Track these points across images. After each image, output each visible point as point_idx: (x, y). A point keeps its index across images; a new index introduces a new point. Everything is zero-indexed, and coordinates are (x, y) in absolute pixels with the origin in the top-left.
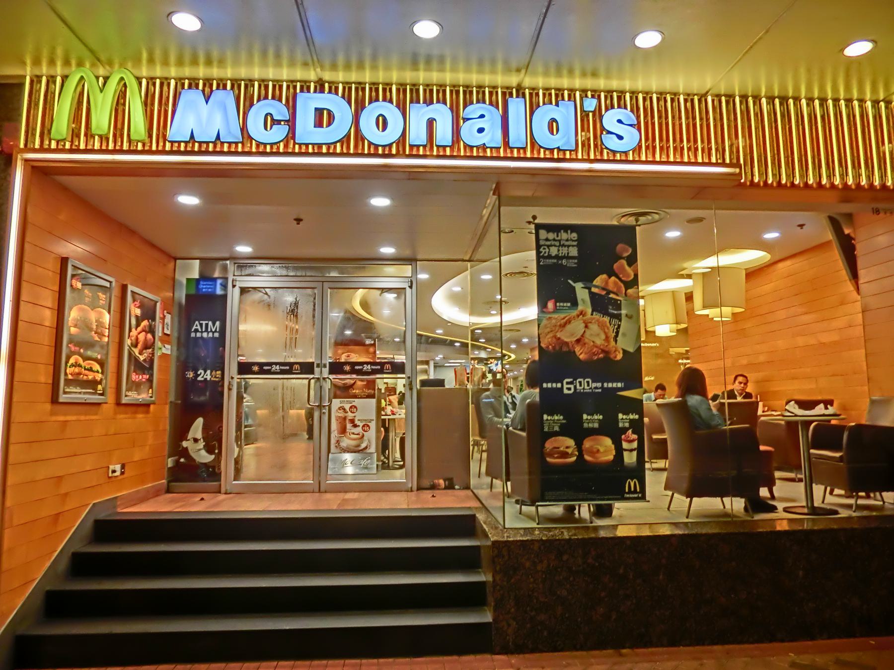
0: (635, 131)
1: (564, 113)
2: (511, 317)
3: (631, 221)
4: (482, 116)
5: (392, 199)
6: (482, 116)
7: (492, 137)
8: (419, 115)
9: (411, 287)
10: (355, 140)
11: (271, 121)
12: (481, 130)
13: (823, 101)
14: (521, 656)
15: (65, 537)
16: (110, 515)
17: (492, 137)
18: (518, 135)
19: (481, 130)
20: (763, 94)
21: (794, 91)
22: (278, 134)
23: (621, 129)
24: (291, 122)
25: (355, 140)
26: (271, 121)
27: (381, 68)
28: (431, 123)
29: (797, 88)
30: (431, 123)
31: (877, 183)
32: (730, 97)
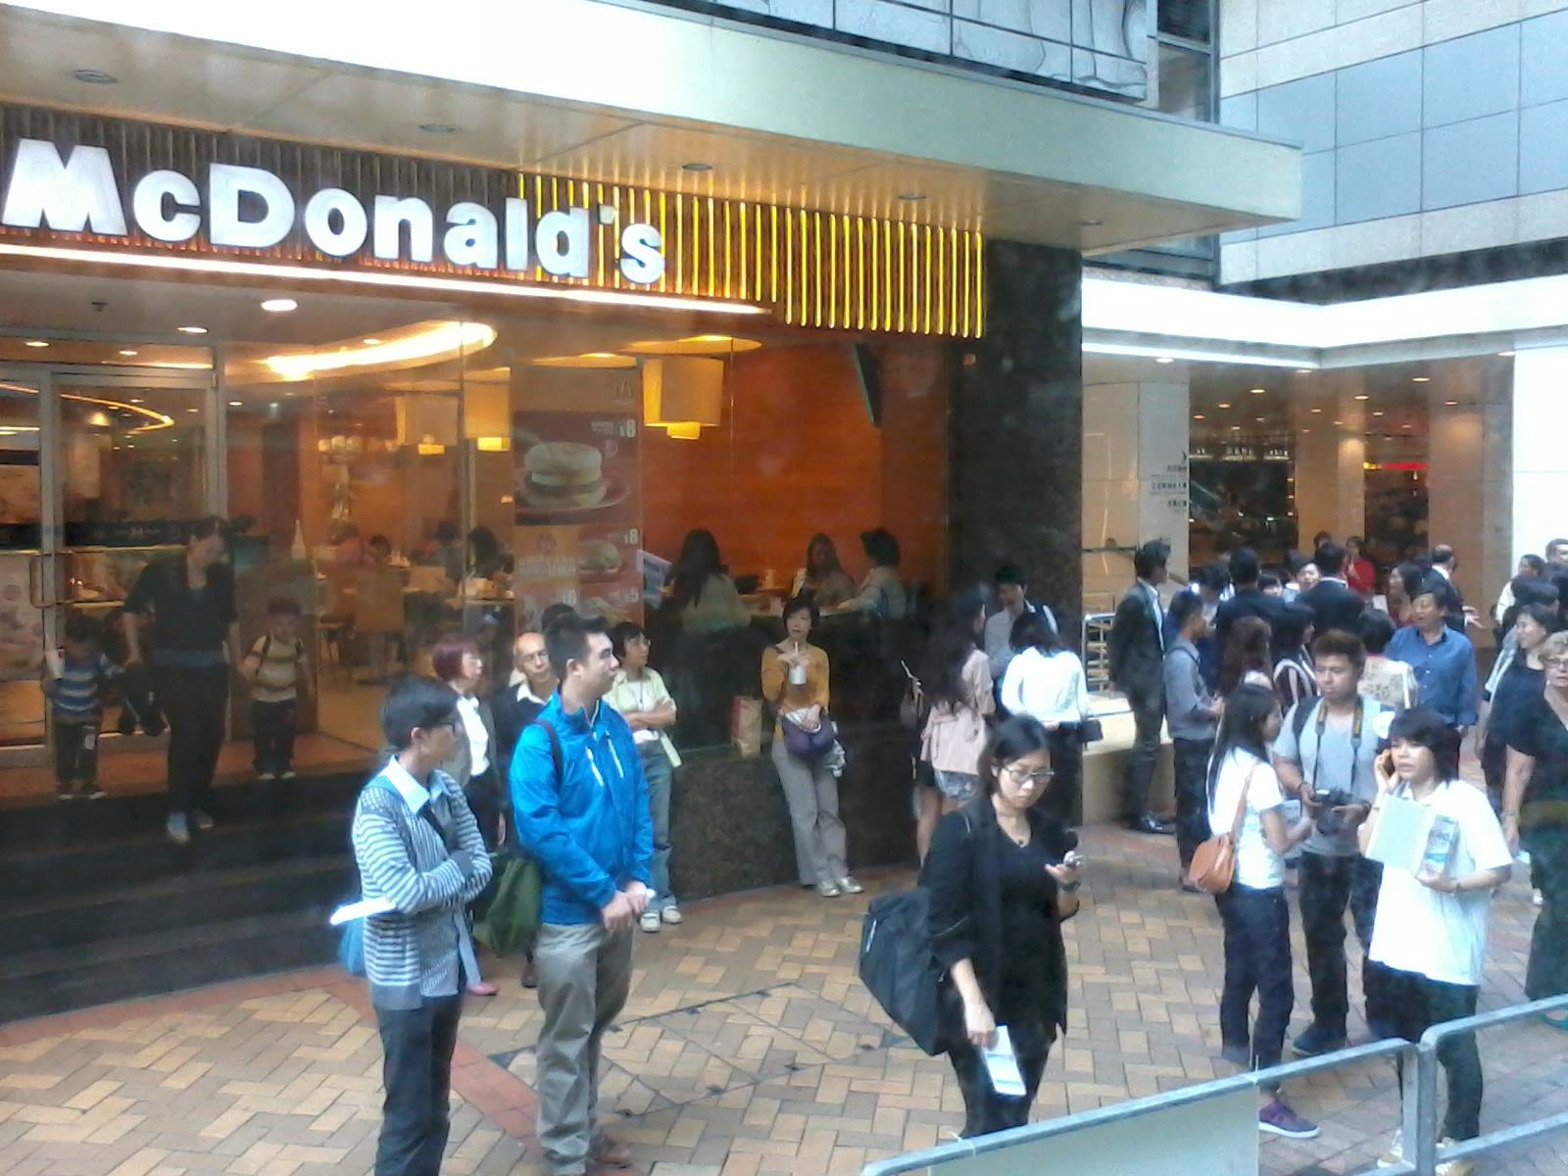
0: (628, 249)
1: (575, 224)
2: (1110, 472)
3: (1104, 587)
4: (472, 222)
5: (261, 309)
6: (472, 222)
7: (487, 258)
8: (390, 210)
10: (296, 246)
11: (170, 207)
12: (470, 243)
13: (867, 223)
14: (1154, 193)
15: (36, 749)
17: (487, 258)
18: (517, 256)
19: (470, 243)
20: (803, 205)
21: (970, 226)
22: (183, 228)
23: (644, 251)
24: (202, 210)
25: (296, 246)
26: (170, 207)
27: (727, 182)
28: (404, 229)
29: (840, 202)
30: (404, 229)
31: (901, 329)
32: (766, 208)
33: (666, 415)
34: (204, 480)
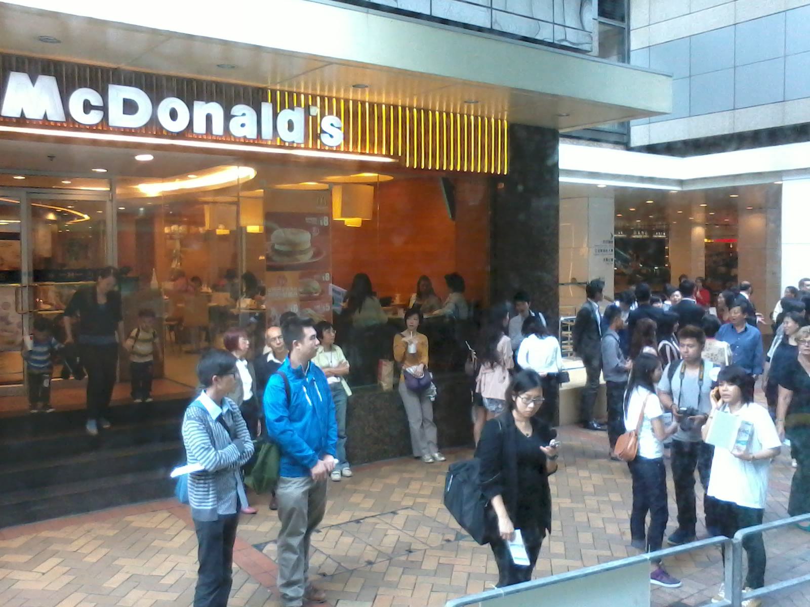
0: (324, 129)
1: (297, 116)
4: (244, 115)
5: (135, 160)
6: (244, 115)
7: (251, 133)
8: (202, 109)
9: (111, 201)
10: (153, 127)
11: (88, 107)
12: (243, 125)
13: (448, 115)
16: (674, 500)
17: (251, 133)
18: (267, 132)
19: (243, 125)
20: (415, 106)
21: (501, 116)
22: (94, 117)
23: (333, 129)
24: (104, 109)
25: (153, 127)
26: (88, 107)
27: (376, 94)
28: (209, 118)
29: (434, 104)
30: (209, 118)
31: (466, 170)
32: (396, 107)
33: (344, 214)
34: (105, 248)
